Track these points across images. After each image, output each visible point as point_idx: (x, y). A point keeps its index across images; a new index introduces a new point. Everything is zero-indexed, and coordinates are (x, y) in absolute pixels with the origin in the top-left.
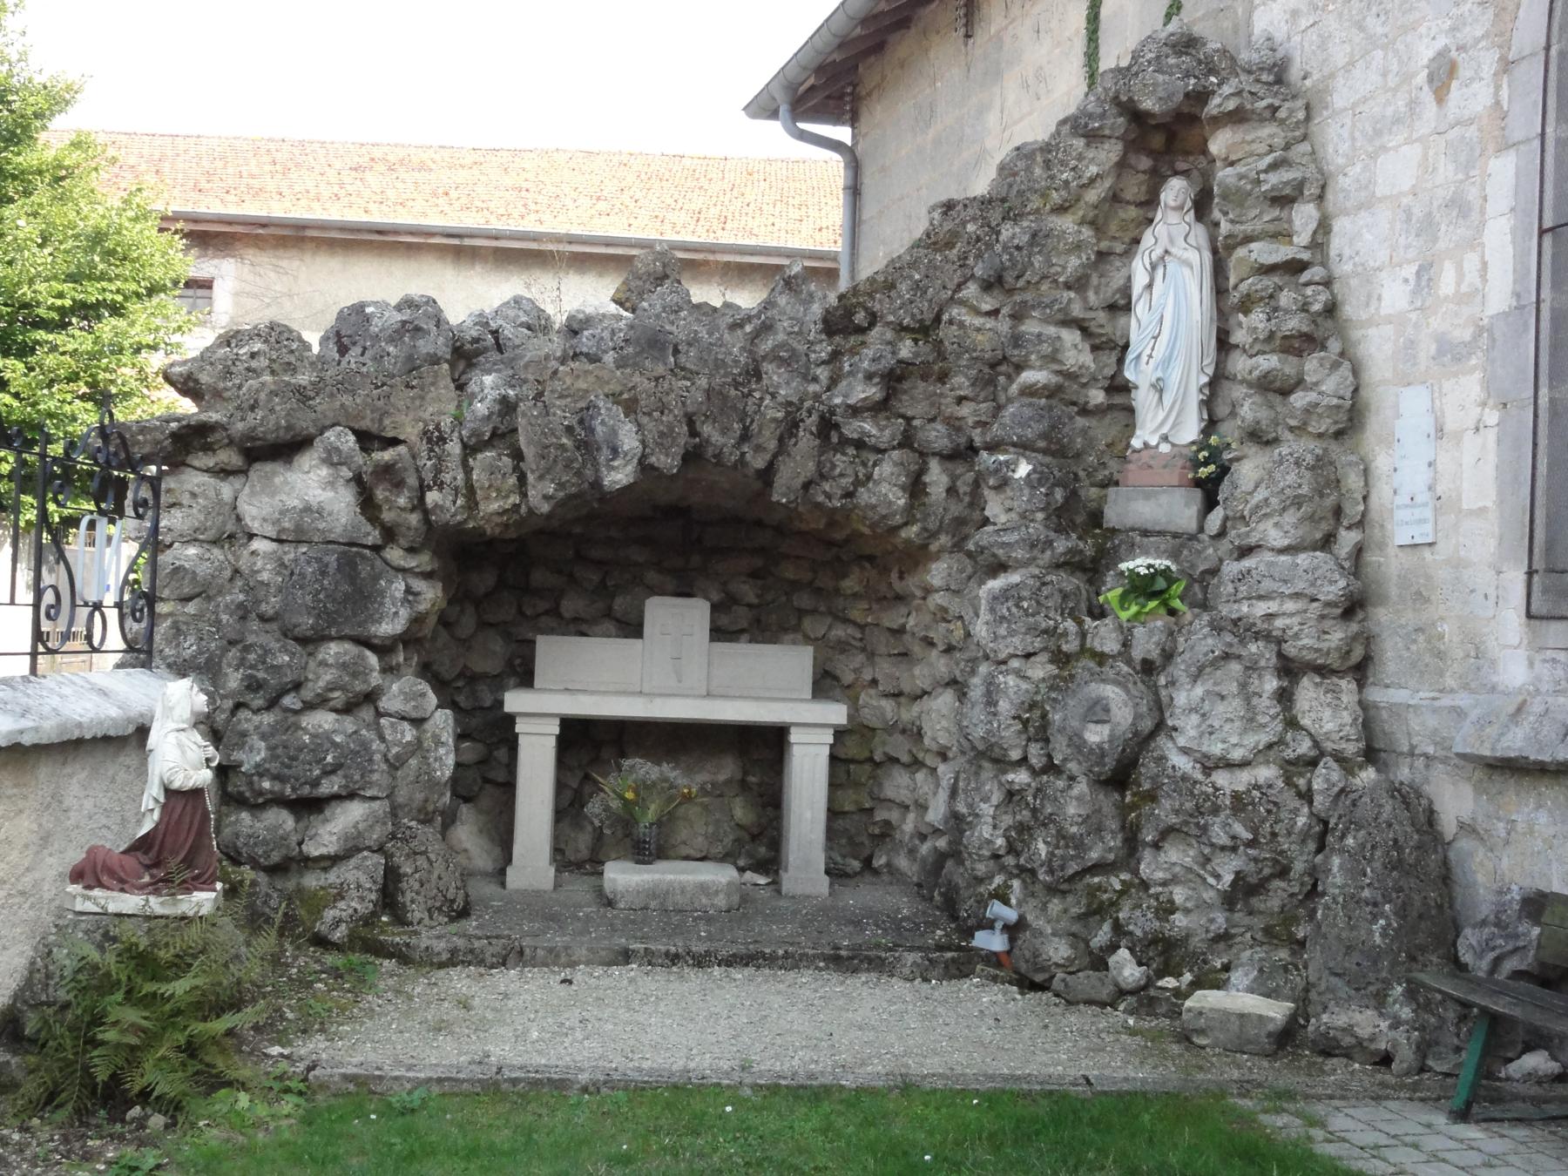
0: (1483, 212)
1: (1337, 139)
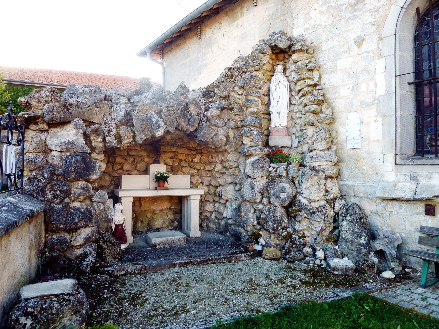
0: (375, 72)
1: (323, 57)
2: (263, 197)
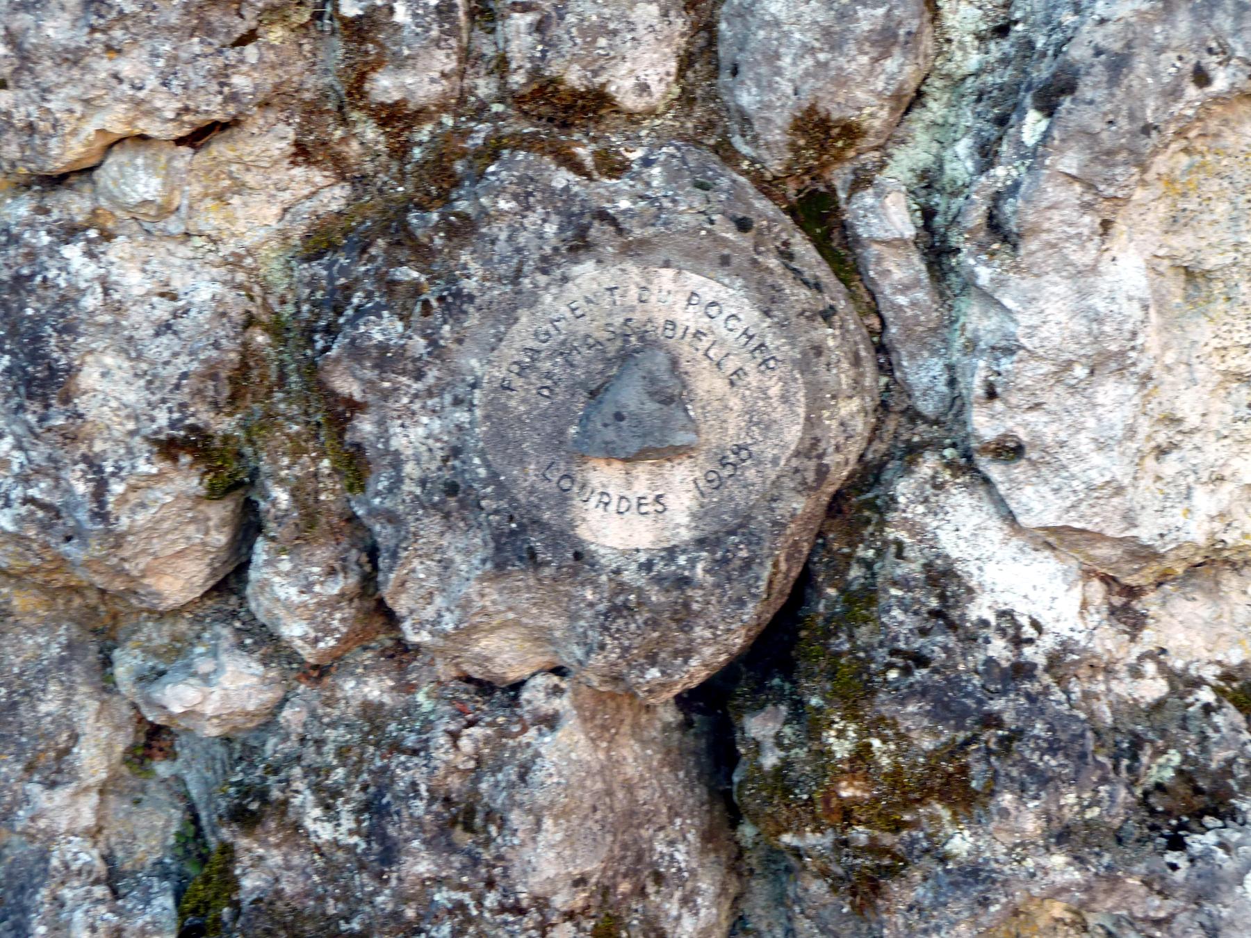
2: (249, 525)
